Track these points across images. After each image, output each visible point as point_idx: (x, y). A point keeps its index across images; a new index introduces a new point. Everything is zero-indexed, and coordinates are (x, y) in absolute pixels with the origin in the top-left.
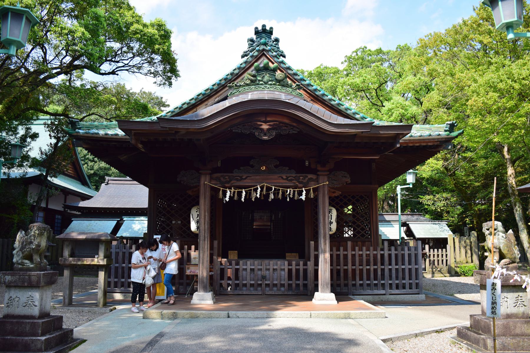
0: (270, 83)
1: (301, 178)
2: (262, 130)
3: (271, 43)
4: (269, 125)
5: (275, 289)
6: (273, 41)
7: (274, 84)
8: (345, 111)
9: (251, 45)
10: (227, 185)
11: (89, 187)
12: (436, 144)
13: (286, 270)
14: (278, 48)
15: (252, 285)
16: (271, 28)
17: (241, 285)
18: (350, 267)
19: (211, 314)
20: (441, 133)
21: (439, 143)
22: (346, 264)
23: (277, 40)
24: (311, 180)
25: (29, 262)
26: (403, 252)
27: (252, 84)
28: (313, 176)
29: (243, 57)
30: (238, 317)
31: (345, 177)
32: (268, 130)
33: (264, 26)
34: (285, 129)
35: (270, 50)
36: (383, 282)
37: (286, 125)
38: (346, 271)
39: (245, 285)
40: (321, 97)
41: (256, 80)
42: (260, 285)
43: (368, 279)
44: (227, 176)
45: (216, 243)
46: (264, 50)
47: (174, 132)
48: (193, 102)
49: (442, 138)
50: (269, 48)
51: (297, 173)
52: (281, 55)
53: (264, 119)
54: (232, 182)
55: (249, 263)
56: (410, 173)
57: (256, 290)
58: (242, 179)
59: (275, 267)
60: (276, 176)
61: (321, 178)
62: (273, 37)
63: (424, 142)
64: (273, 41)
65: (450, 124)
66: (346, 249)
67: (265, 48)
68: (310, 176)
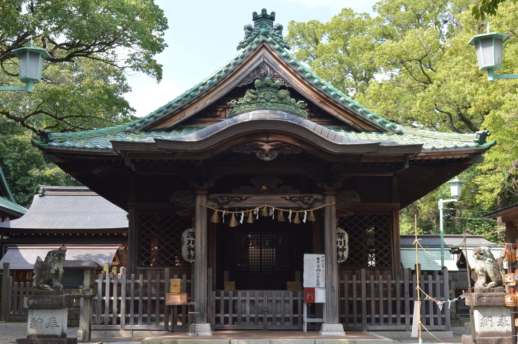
0: (272, 100)
2: (264, 150)
3: (273, 32)
4: (272, 145)
6: (276, 30)
7: (276, 102)
9: (248, 35)
11: (9, 198)
12: (464, 156)
13: (291, 302)
14: (281, 38)
15: (252, 319)
16: (273, 13)
17: (239, 319)
18: (364, 299)
20: (469, 144)
21: (468, 155)
22: (359, 295)
24: (316, 200)
27: (253, 102)
28: (320, 197)
29: (239, 48)
31: (355, 197)
32: (270, 150)
33: (264, 11)
34: (287, 150)
35: (271, 42)
37: (289, 145)
38: (359, 303)
39: (244, 319)
41: (257, 98)
42: (261, 319)
43: (386, 312)
44: (225, 196)
45: (211, 270)
46: (264, 41)
47: (171, 153)
49: (471, 150)
50: (270, 39)
53: (265, 139)
54: (231, 203)
56: (454, 183)
57: (257, 324)
58: (241, 200)
59: (278, 299)
61: (328, 199)
62: (275, 23)
64: (276, 30)
66: (359, 278)
67: (266, 39)
68: (316, 196)
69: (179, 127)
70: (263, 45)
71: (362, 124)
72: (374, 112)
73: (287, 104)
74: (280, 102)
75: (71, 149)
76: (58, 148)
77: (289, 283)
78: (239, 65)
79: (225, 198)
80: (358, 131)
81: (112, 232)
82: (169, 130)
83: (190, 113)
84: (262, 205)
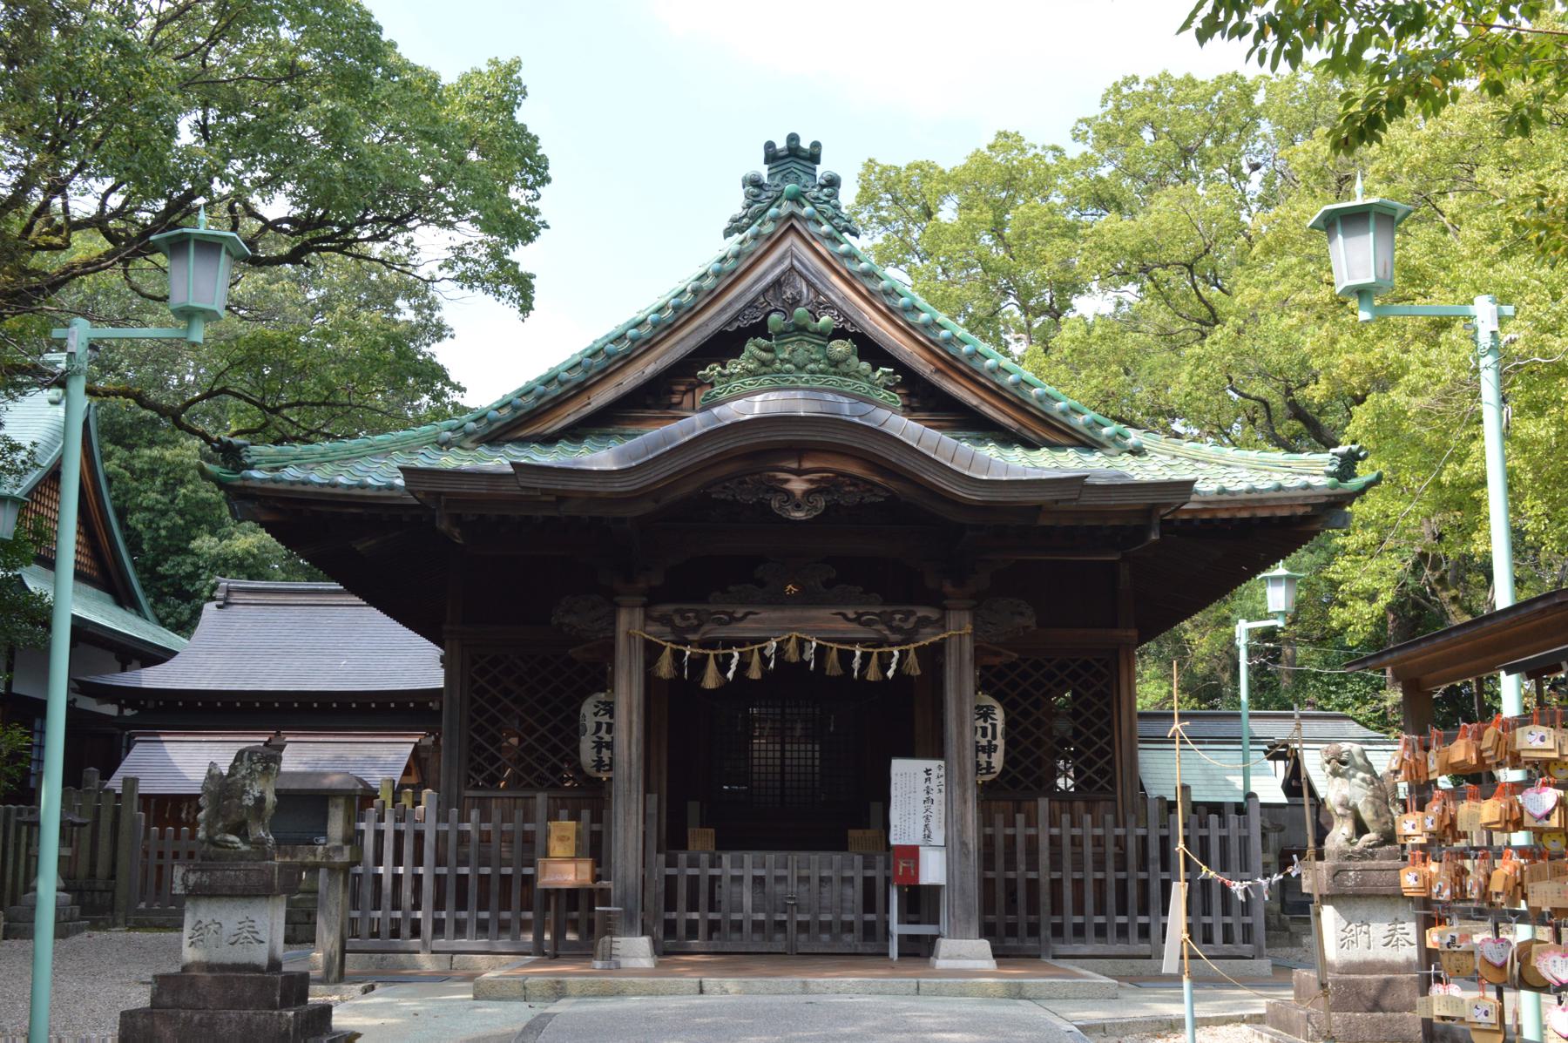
0: (812, 366)
1: (898, 616)
3: (815, 192)
5: (825, 937)
6: (823, 186)
7: (822, 372)
8: (1038, 405)
9: (753, 199)
10: (691, 637)
11: (139, 612)
12: (1300, 511)
13: (859, 882)
14: (837, 207)
15: (758, 926)
16: (816, 145)
18: (1044, 875)
20: (1314, 481)
21: (1309, 509)
22: (1033, 864)
24: (924, 622)
26: (1203, 832)
27: (764, 369)
28: (932, 614)
29: (728, 233)
31: (1021, 614)
32: (807, 493)
33: (793, 138)
35: (809, 218)
36: (1143, 919)
38: (1033, 885)
39: (737, 926)
40: (966, 360)
41: (773, 362)
42: (781, 925)
43: (1100, 909)
44: (690, 611)
45: (654, 798)
46: (792, 215)
48: (577, 376)
50: (808, 209)
51: (886, 602)
52: (847, 229)
53: (794, 465)
54: (706, 628)
57: (771, 940)
58: (733, 619)
59: (825, 873)
60: (825, 613)
62: (821, 170)
63: (1264, 507)
64: (823, 186)
66: (1031, 822)
67: (797, 210)
68: (922, 612)
69: (575, 433)
70: (790, 225)
71: (1038, 426)
72: (1067, 396)
75: (299, 487)
77: (853, 834)
78: (728, 275)
80: (1030, 445)
82: (549, 440)
83: (602, 396)
84: (785, 632)
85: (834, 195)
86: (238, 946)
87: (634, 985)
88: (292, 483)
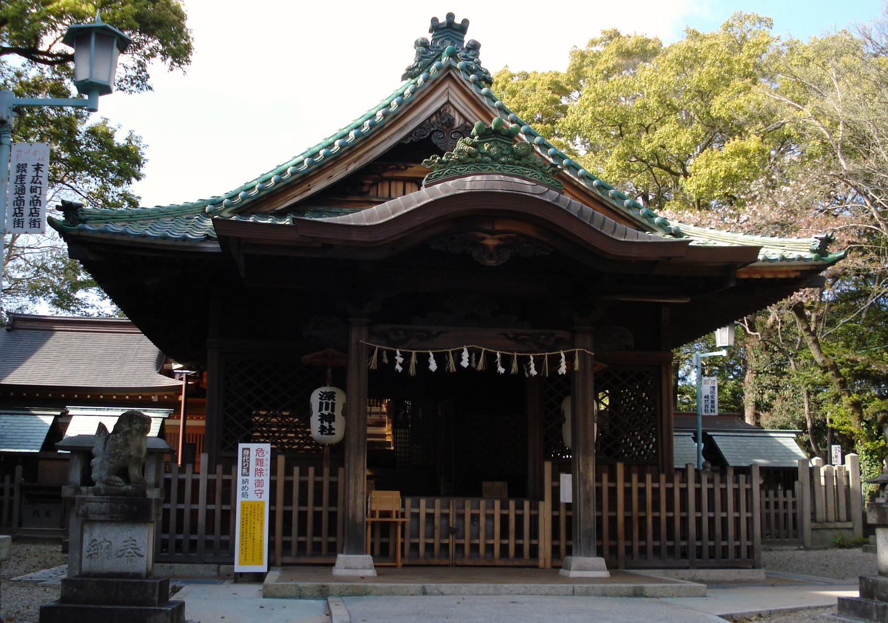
1: (542, 337)
2: (485, 247)
4: (500, 239)
7: (509, 163)
9: (421, 56)
12: (793, 275)
14: (479, 63)
16: (466, 22)
19: (391, 588)
20: (803, 254)
21: (798, 274)
23: (475, 47)
25: (120, 480)
27: (470, 160)
30: (442, 594)
32: (498, 247)
33: (450, 16)
41: (476, 155)
46: (450, 67)
47: (320, 245)
53: (489, 228)
55: (423, 502)
62: (467, 38)
65: (821, 239)
67: (453, 63)
68: (559, 334)
70: (448, 75)
73: (529, 167)
74: (517, 162)
75: (119, 238)
76: (95, 235)
77: (486, 485)
78: (407, 105)
79: (401, 332)
81: (145, 394)
83: (320, 184)
85: (477, 55)
86: (124, 559)
87: (376, 588)
88: (115, 234)
